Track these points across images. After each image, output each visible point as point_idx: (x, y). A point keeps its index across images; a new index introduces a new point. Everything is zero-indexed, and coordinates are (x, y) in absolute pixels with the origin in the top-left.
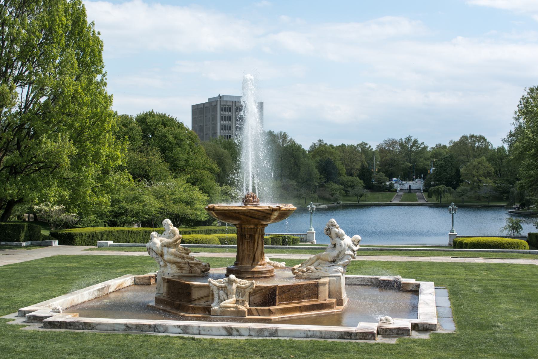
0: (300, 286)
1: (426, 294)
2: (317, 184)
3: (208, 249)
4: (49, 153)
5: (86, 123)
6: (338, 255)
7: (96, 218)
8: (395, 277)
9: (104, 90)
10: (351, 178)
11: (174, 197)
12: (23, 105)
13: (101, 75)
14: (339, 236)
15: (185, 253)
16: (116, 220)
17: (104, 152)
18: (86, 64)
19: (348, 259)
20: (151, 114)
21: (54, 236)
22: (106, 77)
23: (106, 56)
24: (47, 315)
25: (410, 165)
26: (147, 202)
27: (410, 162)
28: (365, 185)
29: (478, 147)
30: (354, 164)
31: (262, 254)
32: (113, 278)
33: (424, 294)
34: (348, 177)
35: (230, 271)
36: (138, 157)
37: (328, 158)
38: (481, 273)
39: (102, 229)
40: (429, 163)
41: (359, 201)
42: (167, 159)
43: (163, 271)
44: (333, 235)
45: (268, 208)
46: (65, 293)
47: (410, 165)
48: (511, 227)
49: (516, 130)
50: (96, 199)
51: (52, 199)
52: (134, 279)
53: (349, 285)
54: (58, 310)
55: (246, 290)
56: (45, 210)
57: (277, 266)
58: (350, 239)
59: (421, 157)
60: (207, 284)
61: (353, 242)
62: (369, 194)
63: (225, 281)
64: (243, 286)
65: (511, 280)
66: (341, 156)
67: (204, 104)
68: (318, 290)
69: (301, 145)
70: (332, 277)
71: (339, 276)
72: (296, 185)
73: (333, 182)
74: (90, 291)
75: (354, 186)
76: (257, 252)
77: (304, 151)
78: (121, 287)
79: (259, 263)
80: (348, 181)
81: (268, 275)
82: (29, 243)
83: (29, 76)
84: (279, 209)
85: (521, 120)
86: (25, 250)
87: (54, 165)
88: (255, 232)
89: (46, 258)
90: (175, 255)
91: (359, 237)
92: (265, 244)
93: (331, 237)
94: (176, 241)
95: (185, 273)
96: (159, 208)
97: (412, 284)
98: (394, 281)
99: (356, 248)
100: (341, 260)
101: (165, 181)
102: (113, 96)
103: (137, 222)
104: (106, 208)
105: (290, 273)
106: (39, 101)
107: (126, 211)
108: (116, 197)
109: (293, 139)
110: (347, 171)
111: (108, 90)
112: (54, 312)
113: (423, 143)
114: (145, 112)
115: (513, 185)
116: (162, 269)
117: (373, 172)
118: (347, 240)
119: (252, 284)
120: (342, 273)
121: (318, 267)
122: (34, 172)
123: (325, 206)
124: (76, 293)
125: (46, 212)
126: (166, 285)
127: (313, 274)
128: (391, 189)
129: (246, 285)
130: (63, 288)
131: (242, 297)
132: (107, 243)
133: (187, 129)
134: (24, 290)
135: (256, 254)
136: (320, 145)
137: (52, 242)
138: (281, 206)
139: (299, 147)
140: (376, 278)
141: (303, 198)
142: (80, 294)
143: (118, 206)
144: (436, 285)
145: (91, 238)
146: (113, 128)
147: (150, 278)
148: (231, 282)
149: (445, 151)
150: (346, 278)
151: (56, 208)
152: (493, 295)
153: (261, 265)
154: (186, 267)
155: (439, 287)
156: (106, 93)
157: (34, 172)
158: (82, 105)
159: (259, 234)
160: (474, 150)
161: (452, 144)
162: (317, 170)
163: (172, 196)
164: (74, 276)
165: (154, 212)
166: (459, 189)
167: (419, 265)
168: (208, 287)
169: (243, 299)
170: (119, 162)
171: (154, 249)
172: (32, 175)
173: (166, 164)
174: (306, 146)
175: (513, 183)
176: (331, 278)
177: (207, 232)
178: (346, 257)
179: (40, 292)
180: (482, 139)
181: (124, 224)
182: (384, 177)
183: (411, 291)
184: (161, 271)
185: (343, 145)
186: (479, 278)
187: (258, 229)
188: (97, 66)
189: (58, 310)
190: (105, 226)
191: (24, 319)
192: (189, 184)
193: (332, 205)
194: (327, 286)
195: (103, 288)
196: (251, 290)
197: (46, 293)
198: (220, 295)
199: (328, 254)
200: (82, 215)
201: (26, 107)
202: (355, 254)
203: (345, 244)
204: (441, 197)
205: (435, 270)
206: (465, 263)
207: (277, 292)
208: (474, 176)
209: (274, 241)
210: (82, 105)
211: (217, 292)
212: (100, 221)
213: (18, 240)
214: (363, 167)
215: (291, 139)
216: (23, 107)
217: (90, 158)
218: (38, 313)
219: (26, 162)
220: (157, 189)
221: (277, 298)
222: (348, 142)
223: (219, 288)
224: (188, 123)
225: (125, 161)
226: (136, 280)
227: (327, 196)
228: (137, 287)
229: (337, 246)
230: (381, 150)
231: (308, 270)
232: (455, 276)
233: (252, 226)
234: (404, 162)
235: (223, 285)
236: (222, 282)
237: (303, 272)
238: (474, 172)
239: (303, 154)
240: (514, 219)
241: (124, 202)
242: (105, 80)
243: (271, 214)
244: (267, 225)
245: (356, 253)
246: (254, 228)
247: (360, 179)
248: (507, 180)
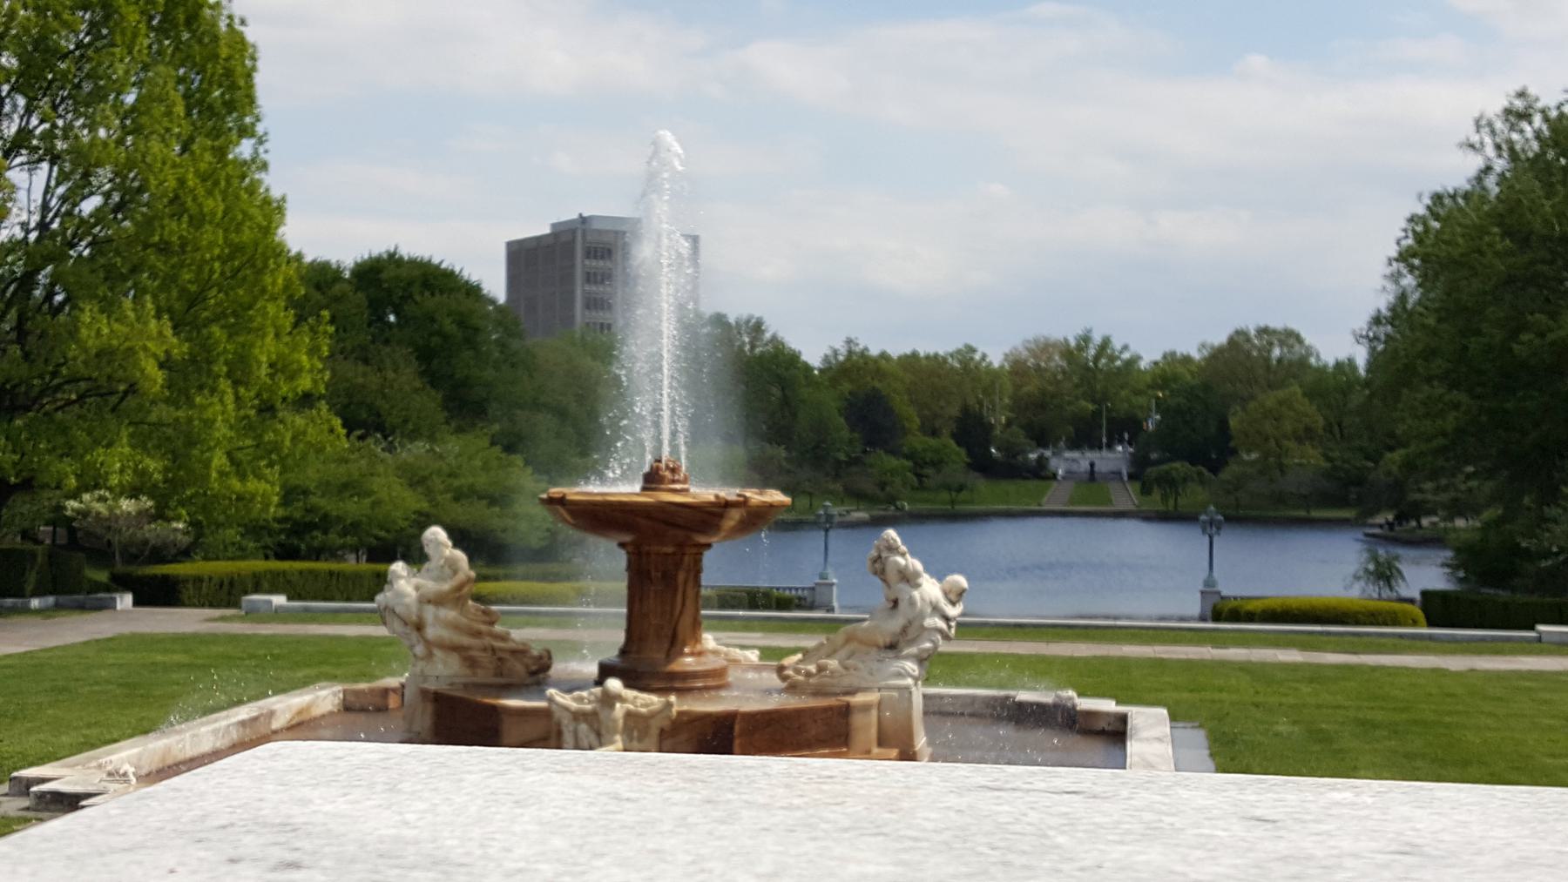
0: (798, 713)
1: (1147, 740)
2: (842, 457)
3: (546, 619)
4: (104, 354)
5: (212, 271)
6: (904, 630)
7: (242, 535)
8: (1059, 693)
9: (260, 182)
10: (933, 442)
11: (456, 483)
12: (35, 218)
13: (253, 141)
14: (909, 578)
15: (485, 623)
16: (296, 542)
17: (262, 353)
18: (210, 107)
19: (932, 641)
20: (393, 259)
21: (122, 583)
22: (267, 145)
23: (263, 81)
24: (91, 789)
25: (1091, 407)
26: (383, 495)
27: (1094, 401)
28: (968, 460)
29: (1280, 361)
30: (942, 403)
31: (696, 626)
32: (284, 691)
33: (1141, 740)
34: (927, 439)
35: (606, 671)
36: (355, 373)
37: (874, 388)
38: (1296, 689)
39: (260, 565)
40: (1142, 400)
41: (953, 502)
42: (432, 378)
43: (422, 671)
44: (892, 575)
45: (712, 498)
46: (146, 732)
47: (1091, 407)
48: (1371, 573)
49: (1392, 309)
50: (236, 484)
51: (114, 480)
52: (341, 696)
53: (934, 713)
54: (125, 774)
56: (98, 513)
59: (1122, 388)
60: (542, 704)
61: (946, 594)
62: (982, 485)
63: (592, 698)
64: (643, 710)
65: (1382, 708)
67: (538, 239)
68: (848, 724)
69: (800, 352)
71: (907, 688)
72: (786, 459)
74: (217, 725)
75: (941, 461)
77: (807, 368)
78: (305, 717)
79: (687, 650)
80: (924, 450)
81: (715, 679)
82: (51, 600)
83: (48, 136)
84: (743, 503)
85: (1409, 281)
86: (38, 619)
87: (122, 388)
88: (678, 565)
89: (97, 641)
90: (456, 627)
91: (961, 580)
92: (706, 607)
93: (884, 581)
94: (459, 588)
95: (483, 676)
96: (414, 513)
97: (1107, 714)
98: (1056, 706)
99: (953, 611)
100: (912, 642)
101: (432, 438)
102: (289, 198)
103: (355, 550)
104: (266, 506)
105: (772, 679)
106: (77, 210)
107: (325, 517)
108: (294, 479)
109: (780, 335)
110: (923, 424)
111: (274, 183)
112: (112, 781)
113: (1126, 348)
114: (375, 253)
115: (1376, 462)
116: (421, 664)
117: (991, 427)
118: (930, 589)
119: (669, 705)
120: (916, 679)
121: (850, 662)
122: (65, 405)
123: (862, 515)
124: (179, 732)
125: (101, 519)
126: (430, 708)
128: (1040, 472)
129: (652, 708)
130: (143, 719)
132: (270, 602)
133: (493, 302)
134: (29, 725)
136: (850, 352)
137: (114, 600)
138: (748, 494)
139: (793, 359)
140: (1007, 698)
141: (804, 492)
142: (188, 735)
143: (301, 504)
144: (1173, 717)
145: (226, 587)
146: (286, 287)
147: (385, 692)
148: (609, 700)
149: (1188, 370)
150: (925, 696)
151: (127, 505)
152: (1335, 746)
153: (692, 654)
154: (484, 657)
155: (1181, 725)
156: (267, 190)
157: (65, 405)
158: (198, 221)
159: (688, 571)
160: (1268, 367)
161: (1206, 353)
162: (842, 420)
163: (450, 480)
164: (175, 687)
165: (405, 524)
166: (1225, 475)
167: (1124, 664)
168: (545, 714)
170: (305, 383)
171: (398, 610)
172: (59, 414)
173: (433, 393)
174: (813, 355)
175: (1375, 458)
176: (885, 693)
177: (544, 578)
178: (926, 634)
179: (76, 728)
180: (1290, 337)
181: (316, 554)
182: (1021, 438)
183: (1102, 733)
184: (418, 669)
185: (915, 355)
186: (1291, 700)
187: (686, 558)
188: (241, 118)
189: (125, 774)
190: (267, 558)
191: (25, 802)
192: (498, 448)
193: (882, 513)
194: (874, 713)
195: (255, 719)
196: (666, 724)
197: (94, 732)
198: (581, 735)
200: (202, 527)
201: (43, 226)
202: (950, 627)
203: (923, 599)
204: (1177, 494)
205: (1167, 679)
206: (1250, 662)
207: (737, 728)
208: (1267, 439)
209: (729, 599)
210: (198, 221)
211: (571, 728)
212: (251, 545)
213: (20, 594)
214: (965, 410)
215: (774, 338)
216: (32, 225)
217: (220, 368)
218: (68, 783)
219: (41, 377)
220: (411, 460)
222: (925, 348)
223: (578, 716)
224: (495, 285)
225: (322, 378)
226: (348, 697)
227: (868, 486)
228: (351, 717)
229: (903, 605)
230: (1018, 369)
231: (821, 669)
232: (1224, 696)
233: (670, 550)
234: (1077, 398)
235: (588, 707)
236: (584, 700)
237: (808, 674)
238: (1268, 427)
239: (806, 377)
240: (1381, 552)
241: (320, 493)
242: (263, 156)
243: (721, 516)
244: (709, 546)
245: (953, 624)
246: (674, 554)
247: (959, 444)
248: (1361, 449)
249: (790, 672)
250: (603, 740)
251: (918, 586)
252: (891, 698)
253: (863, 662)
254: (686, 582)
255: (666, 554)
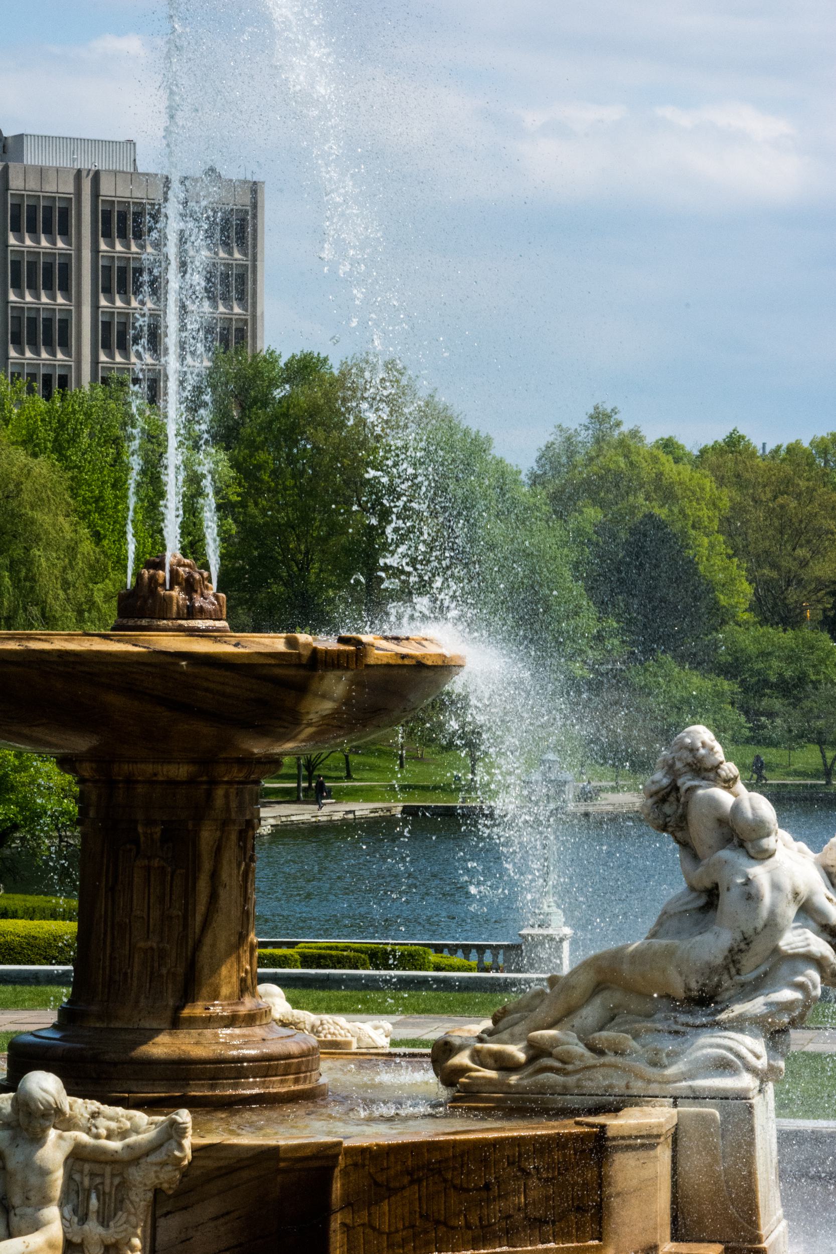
19: (801, 987)
55: (135, 1175)
57: (335, 1044)
58: (811, 855)
64: (115, 1145)
66: (725, 503)
70: (696, 1097)
71: (742, 1096)
73: (681, 659)
76: (208, 940)
127: (571, 1080)
129: (133, 1139)
131: (104, 1222)
135: (206, 949)
153: (232, 1021)
169: (111, 1235)
178: (784, 970)
187: (220, 792)
194: (664, 1154)
196: (169, 1178)
199: (669, 953)
203: (776, 887)
207: (337, 1187)
221: (336, 1222)
229: (729, 901)
231: (537, 1051)
233: (182, 771)
237: (504, 1064)
246: (191, 781)
249: (463, 1059)
250: (15, 1220)
251: (764, 855)
252: (704, 1120)
253: (636, 1036)
254: (218, 851)
255: (172, 783)
